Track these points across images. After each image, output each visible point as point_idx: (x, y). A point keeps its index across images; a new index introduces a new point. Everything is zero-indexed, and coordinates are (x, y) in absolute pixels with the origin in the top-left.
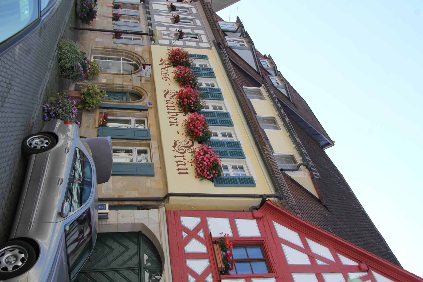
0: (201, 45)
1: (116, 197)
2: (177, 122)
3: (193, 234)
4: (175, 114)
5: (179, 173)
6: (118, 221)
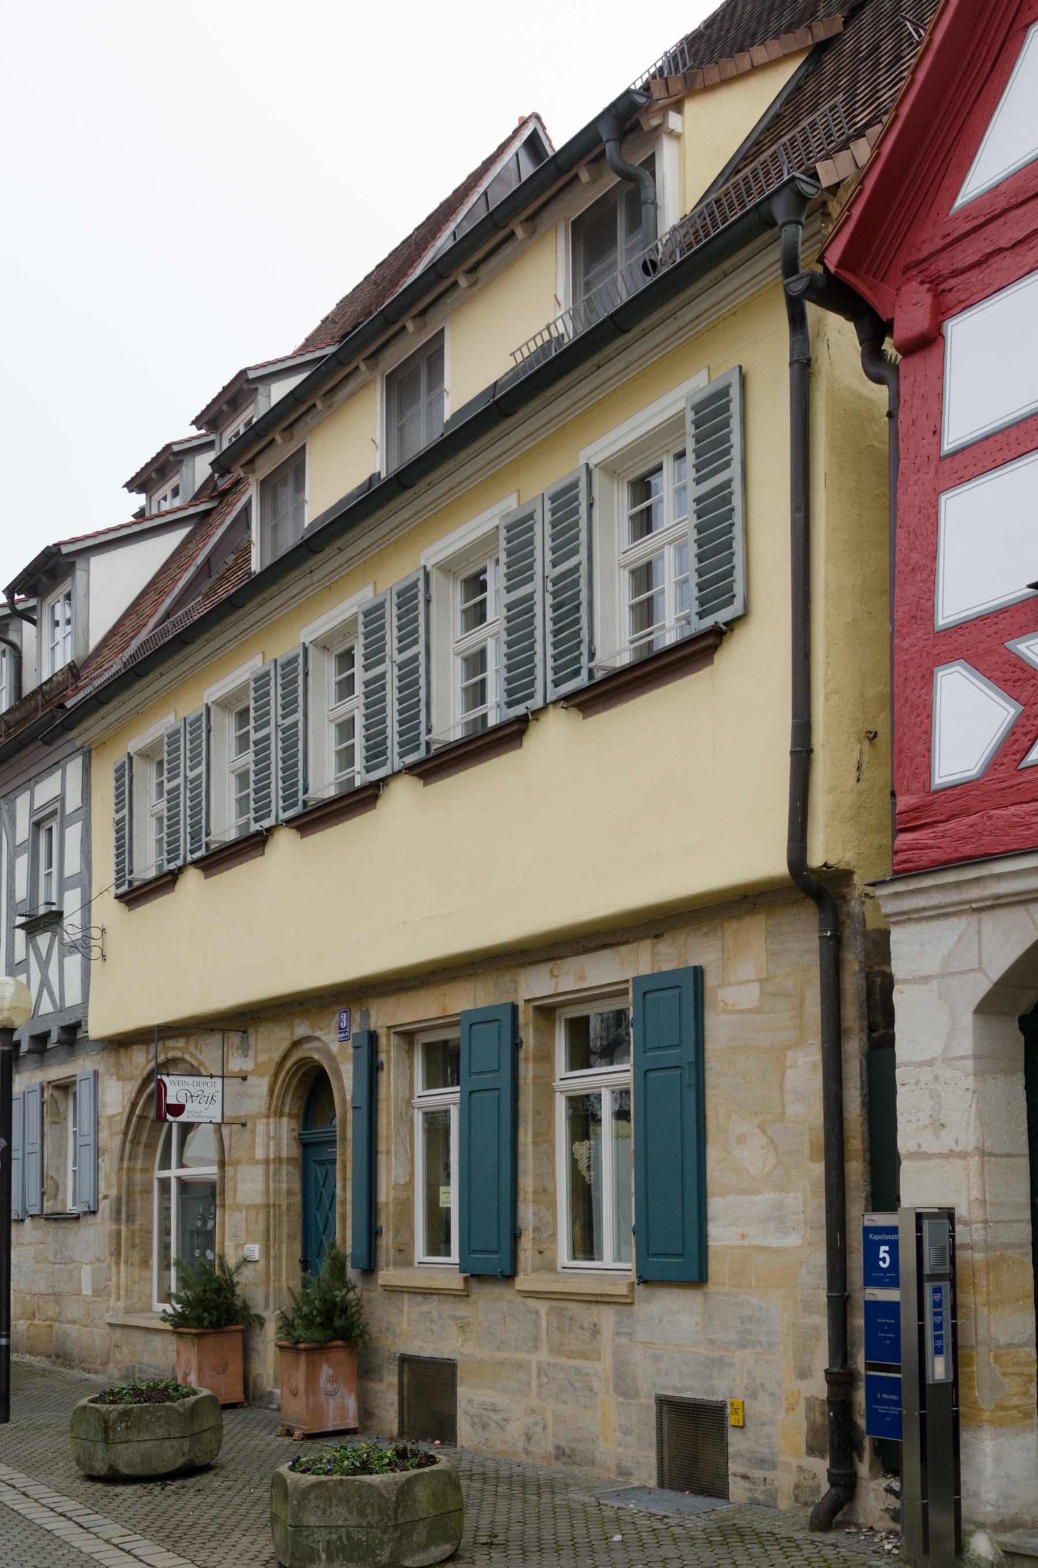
1: (819, 1169)
6: (964, 1155)
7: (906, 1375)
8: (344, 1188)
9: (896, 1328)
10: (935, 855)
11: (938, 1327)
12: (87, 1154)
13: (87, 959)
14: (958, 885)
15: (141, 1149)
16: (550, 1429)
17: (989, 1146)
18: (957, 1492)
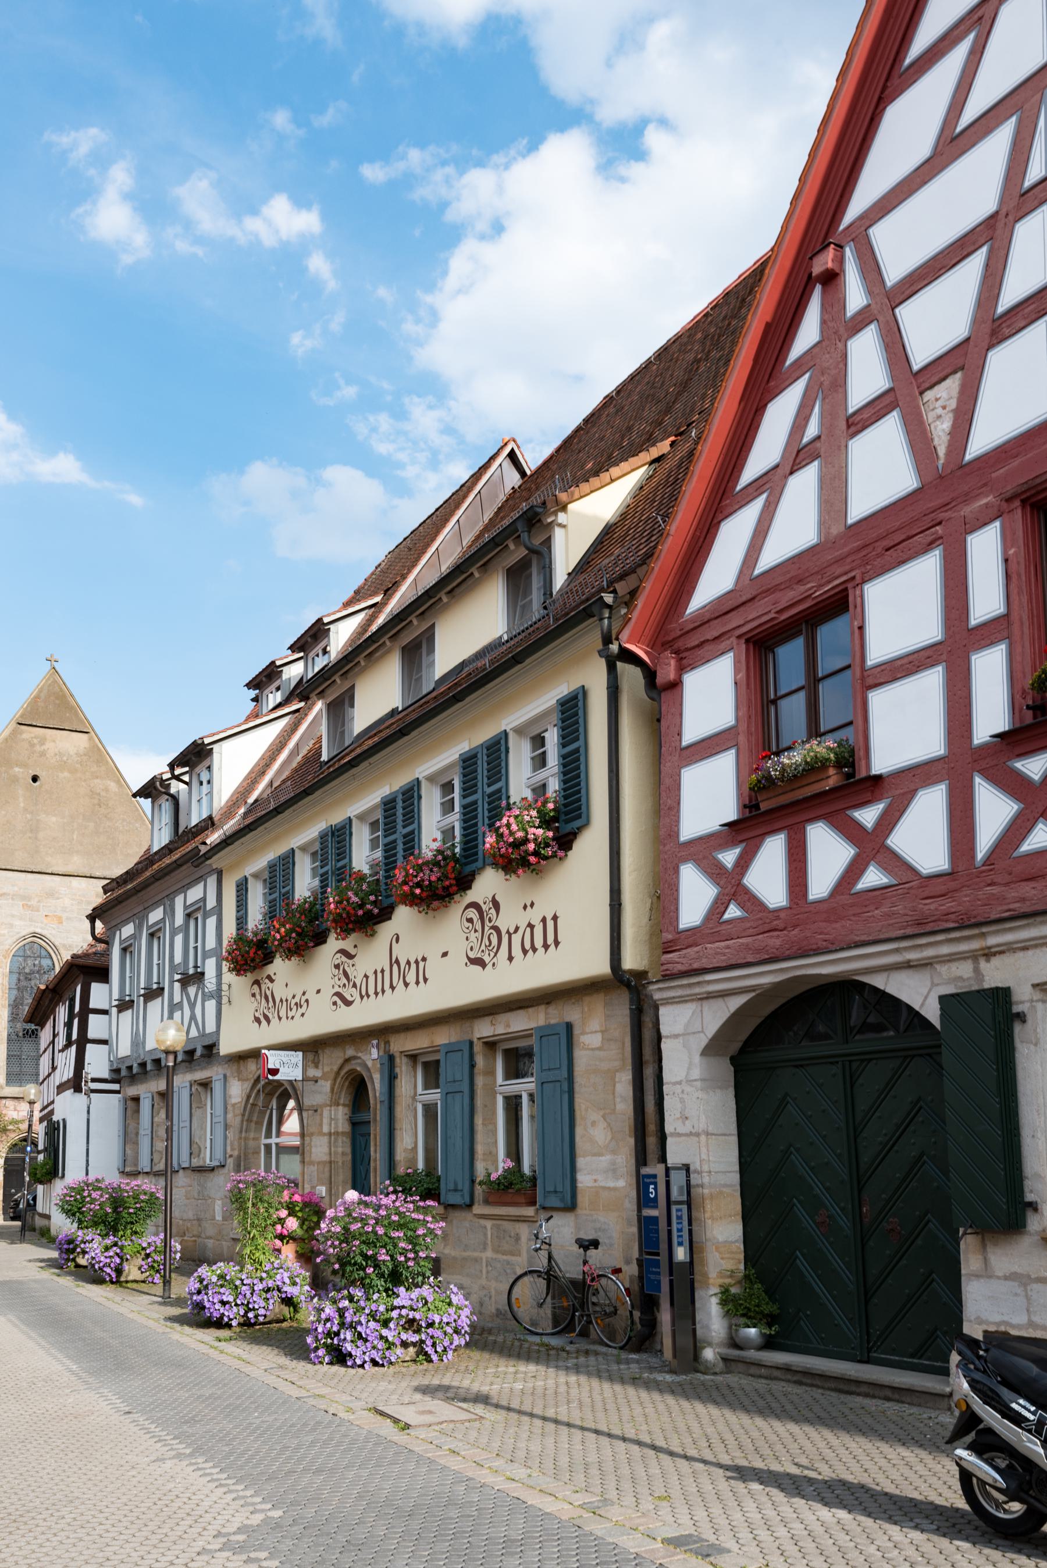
0: (211, 903)
2: (417, 962)
3: (732, 886)
4: (395, 967)
5: (557, 943)
6: (698, 1135)
7: (663, 1258)
8: (376, 1151)
9: (657, 1231)
11: (680, 1230)
12: (219, 1130)
13: (219, 1004)
14: (690, 985)
15: (253, 1125)
16: (493, 1299)
17: (710, 1130)
18: (694, 1324)
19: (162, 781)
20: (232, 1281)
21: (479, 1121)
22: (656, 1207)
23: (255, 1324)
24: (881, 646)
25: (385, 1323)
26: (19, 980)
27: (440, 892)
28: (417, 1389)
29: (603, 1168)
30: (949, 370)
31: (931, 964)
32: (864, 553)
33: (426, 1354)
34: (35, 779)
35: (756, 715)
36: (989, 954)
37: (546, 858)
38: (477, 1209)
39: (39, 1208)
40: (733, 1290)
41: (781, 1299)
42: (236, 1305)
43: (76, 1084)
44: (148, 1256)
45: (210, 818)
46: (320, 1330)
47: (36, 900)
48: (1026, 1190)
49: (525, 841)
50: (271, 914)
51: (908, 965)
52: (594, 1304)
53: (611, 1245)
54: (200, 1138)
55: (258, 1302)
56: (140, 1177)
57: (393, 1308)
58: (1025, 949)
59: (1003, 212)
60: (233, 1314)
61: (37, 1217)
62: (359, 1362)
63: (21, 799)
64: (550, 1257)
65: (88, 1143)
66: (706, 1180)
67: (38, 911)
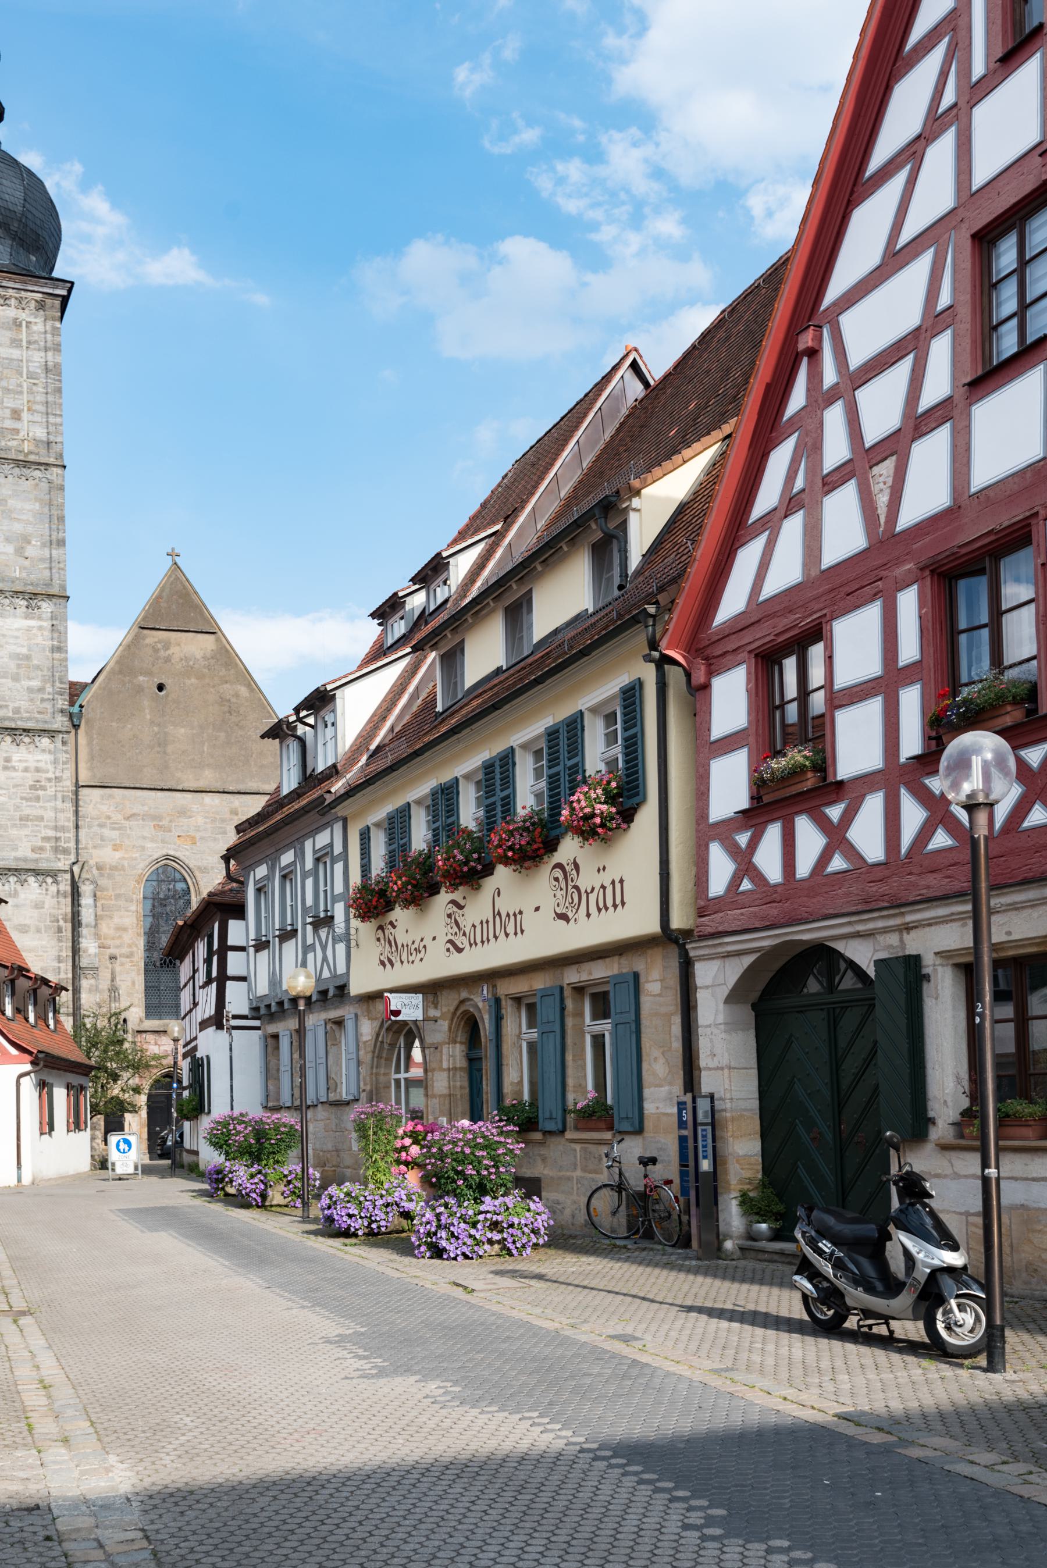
0: (338, 849)
2: (515, 915)
4: (497, 918)
5: (623, 903)
6: (722, 1069)
10: (709, 930)
11: (704, 1146)
12: (353, 1065)
15: (383, 1061)
17: (733, 1064)
19: (289, 724)
20: (356, 1198)
21: (569, 1057)
22: (686, 1128)
23: (378, 1234)
24: (822, 692)
25: (474, 1225)
26: (154, 906)
27: (530, 854)
28: (492, 1272)
29: (661, 1098)
30: (888, 452)
31: (873, 934)
32: (832, 595)
33: (509, 1250)
34: (161, 687)
35: (763, 719)
36: (908, 928)
37: (610, 830)
38: (569, 1135)
39: (187, 1145)
40: (751, 1194)
41: (780, 1198)
42: (361, 1217)
43: (217, 1021)
44: (289, 1182)
45: (334, 766)
46: (422, 1231)
47: (168, 819)
48: (929, 1109)
49: (593, 815)
50: (391, 863)
51: (857, 935)
52: (654, 1211)
53: (669, 1162)
54: (336, 1074)
55: (379, 1215)
56: (283, 1111)
57: (481, 1213)
58: (930, 925)
59: (924, 327)
60: (357, 1224)
61: (185, 1154)
62: (452, 1255)
63: (147, 711)
64: (621, 1174)
65: (231, 1079)
66: (728, 1105)
67: (170, 831)
